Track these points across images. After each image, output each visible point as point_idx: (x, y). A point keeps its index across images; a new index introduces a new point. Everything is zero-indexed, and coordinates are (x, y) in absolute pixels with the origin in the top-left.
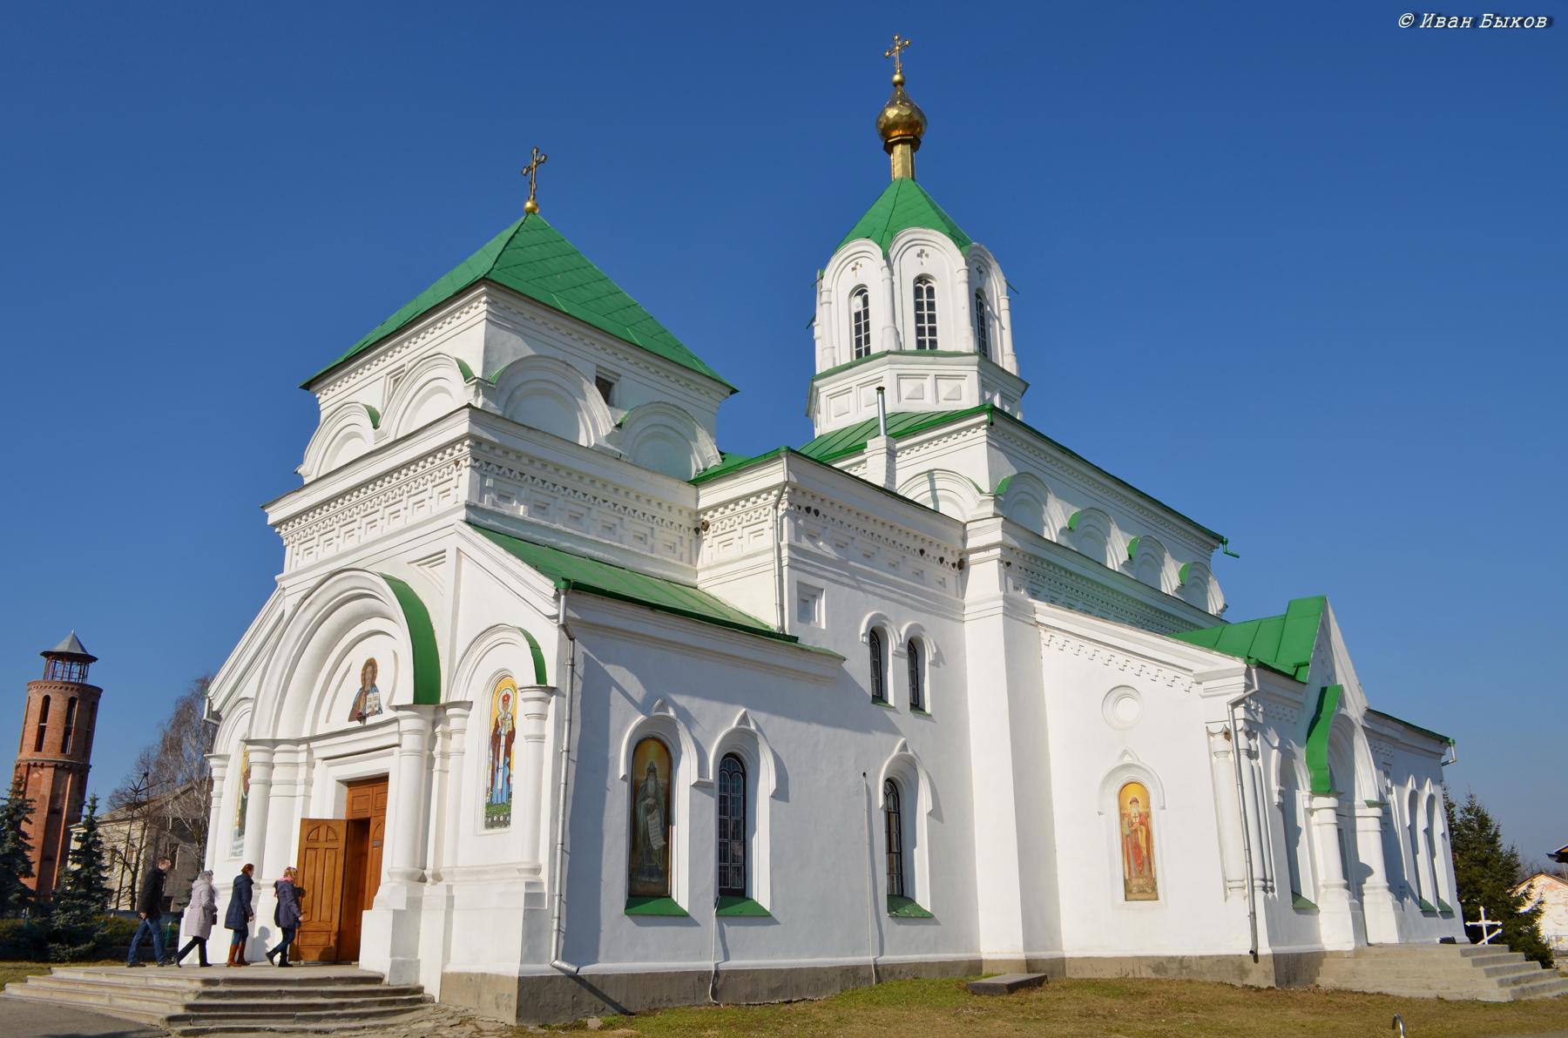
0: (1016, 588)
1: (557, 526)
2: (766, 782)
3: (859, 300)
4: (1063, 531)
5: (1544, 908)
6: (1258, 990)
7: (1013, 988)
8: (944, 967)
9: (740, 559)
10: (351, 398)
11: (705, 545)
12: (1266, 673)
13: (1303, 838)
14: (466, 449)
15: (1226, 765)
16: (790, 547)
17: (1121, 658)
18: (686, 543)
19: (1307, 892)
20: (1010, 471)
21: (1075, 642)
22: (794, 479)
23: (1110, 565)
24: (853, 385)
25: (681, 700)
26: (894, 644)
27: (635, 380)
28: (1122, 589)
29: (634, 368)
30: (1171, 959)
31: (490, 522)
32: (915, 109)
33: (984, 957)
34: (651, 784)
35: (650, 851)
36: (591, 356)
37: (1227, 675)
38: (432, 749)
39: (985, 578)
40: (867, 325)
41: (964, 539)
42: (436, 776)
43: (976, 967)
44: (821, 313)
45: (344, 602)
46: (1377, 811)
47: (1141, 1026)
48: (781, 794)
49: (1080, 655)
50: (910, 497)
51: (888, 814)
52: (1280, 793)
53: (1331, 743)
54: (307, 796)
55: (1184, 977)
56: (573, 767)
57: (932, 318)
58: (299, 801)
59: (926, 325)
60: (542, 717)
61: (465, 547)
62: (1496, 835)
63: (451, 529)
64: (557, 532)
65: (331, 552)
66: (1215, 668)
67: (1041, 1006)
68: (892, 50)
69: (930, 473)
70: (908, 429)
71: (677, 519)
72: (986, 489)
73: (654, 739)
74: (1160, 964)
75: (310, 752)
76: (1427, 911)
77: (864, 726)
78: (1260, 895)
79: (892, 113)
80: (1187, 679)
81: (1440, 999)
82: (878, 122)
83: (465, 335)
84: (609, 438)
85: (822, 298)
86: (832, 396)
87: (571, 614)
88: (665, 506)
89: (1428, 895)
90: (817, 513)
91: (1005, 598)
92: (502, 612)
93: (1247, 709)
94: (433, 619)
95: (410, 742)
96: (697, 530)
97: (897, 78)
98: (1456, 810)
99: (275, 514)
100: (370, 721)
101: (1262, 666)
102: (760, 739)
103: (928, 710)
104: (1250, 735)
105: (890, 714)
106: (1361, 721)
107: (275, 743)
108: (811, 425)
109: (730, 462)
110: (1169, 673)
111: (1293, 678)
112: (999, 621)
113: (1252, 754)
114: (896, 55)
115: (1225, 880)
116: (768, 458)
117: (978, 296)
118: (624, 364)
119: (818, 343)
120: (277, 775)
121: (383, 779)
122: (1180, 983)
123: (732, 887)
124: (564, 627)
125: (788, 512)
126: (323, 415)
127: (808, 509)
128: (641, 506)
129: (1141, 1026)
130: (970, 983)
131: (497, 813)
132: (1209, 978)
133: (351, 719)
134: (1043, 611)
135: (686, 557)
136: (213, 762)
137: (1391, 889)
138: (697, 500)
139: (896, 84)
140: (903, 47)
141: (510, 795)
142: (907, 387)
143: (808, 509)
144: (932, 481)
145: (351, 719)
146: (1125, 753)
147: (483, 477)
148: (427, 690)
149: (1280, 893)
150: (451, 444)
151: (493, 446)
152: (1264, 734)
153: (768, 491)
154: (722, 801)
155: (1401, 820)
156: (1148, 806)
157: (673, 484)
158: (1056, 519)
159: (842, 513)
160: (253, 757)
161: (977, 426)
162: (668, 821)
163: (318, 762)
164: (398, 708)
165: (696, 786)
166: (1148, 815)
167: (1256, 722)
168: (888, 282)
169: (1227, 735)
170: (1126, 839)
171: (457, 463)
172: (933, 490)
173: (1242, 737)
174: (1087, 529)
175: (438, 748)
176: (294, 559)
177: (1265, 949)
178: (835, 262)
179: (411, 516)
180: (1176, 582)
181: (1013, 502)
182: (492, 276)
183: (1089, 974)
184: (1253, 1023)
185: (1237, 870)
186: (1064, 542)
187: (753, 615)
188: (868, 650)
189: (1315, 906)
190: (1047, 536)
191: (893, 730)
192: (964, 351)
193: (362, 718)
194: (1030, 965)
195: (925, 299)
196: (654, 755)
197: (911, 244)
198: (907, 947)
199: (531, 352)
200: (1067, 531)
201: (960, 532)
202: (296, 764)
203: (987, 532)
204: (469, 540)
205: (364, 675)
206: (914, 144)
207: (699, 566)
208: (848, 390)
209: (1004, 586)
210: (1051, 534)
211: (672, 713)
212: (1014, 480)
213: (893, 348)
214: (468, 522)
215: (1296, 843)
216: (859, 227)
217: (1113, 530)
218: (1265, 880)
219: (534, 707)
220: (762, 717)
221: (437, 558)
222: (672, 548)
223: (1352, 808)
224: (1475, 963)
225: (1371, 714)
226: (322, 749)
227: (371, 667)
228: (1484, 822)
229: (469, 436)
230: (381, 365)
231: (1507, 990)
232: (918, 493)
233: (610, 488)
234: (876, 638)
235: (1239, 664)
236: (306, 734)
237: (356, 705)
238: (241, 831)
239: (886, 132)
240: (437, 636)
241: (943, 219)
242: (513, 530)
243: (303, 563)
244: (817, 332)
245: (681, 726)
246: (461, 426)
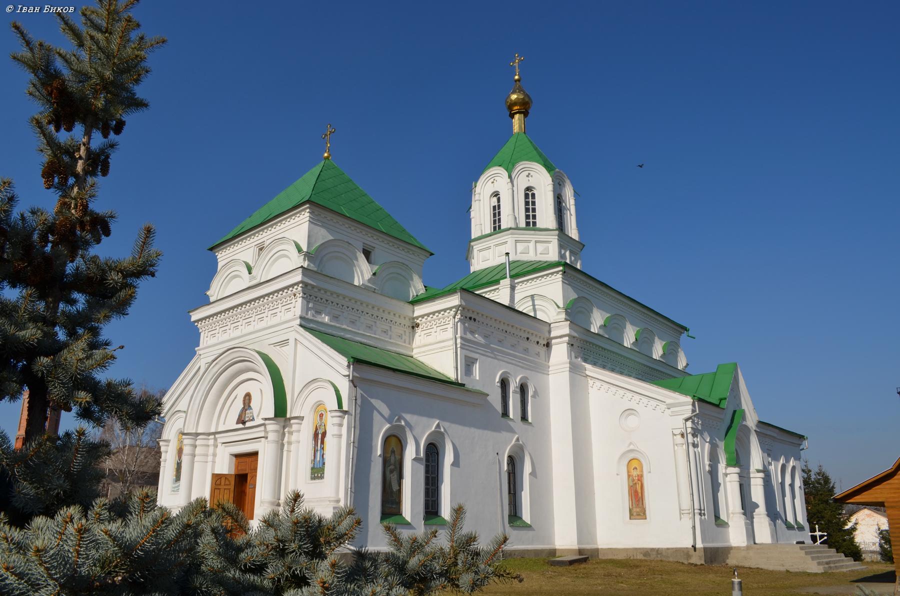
0: (576, 357)
1: (344, 327)
2: (448, 458)
3: (495, 199)
4: (601, 327)
5: (858, 527)
6: (696, 565)
7: (571, 562)
8: (537, 553)
9: (435, 343)
10: (234, 258)
11: (417, 335)
12: (704, 404)
13: (722, 488)
14: (300, 289)
15: (681, 451)
16: (461, 338)
17: (629, 395)
18: (407, 334)
19: (723, 516)
20: (574, 296)
21: (606, 386)
22: (463, 303)
23: (625, 345)
25: (408, 417)
26: (513, 386)
27: (384, 251)
28: (632, 357)
29: (383, 244)
30: (652, 550)
31: (311, 325)
32: (526, 95)
33: (557, 547)
34: (393, 459)
35: (392, 492)
36: (360, 238)
37: (684, 404)
38: (283, 440)
39: (560, 353)
40: (499, 213)
41: (550, 332)
42: (285, 453)
43: (553, 552)
44: (475, 205)
45: (235, 364)
46: (762, 475)
47: (634, 581)
48: (456, 464)
49: (610, 395)
50: (520, 310)
51: (509, 474)
52: (710, 465)
53: (737, 439)
54: (214, 462)
55: (659, 559)
56: (356, 450)
57: (534, 210)
58: (210, 465)
59: (531, 214)
60: (341, 425)
62: (833, 487)
64: (344, 330)
65: (225, 337)
66: (677, 401)
67: (585, 571)
68: (514, 62)
69: (532, 296)
70: (522, 271)
71: (403, 322)
72: (561, 305)
73: (394, 436)
74: (647, 552)
75: (215, 439)
76: (789, 527)
77: (497, 429)
78: (697, 517)
79: (514, 97)
80: (663, 406)
81: (787, 571)
82: (506, 102)
83: (298, 229)
84: (369, 281)
85: (475, 198)
86: (480, 251)
87: (356, 374)
88: (397, 315)
89: (790, 519)
90: (475, 320)
91: (570, 363)
92: (320, 373)
93: (693, 422)
94: (282, 374)
95: (272, 436)
96: (413, 327)
97: (517, 77)
98: (812, 473)
99: (195, 316)
100: (248, 424)
101: (701, 400)
102: (446, 436)
103: (530, 420)
104: (694, 435)
105: (510, 423)
106: (754, 428)
107: (197, 434)
108: (468, 265)
109: (431, 292)
110: (653, 403)
111: (717, 406)
112: (566, 375)
113: (695, 446)
114: (516, 65)
115: (680, 510)
116: (451, 292)
117: (558, 198)
119: (473, 221)
120: (198, 451)
121: (255, 454)
122: (657, 561)
123: (431, 509)
124: (352, 381)
125: (460, 320)
126: (220, 265)
127: (470, 318)
128: (385, 316)
129: (634, 581)
130: (550, 560)
131: (317, 472)
132: (671, 559)
133: (237, 423)
134: (590, 370)
135: (407, 341)
136: (161, 443)
137: (768, 515)
138: (414, 312)
139: (516, 81)
140: (520, 60)
141: (324, 464)
142: (521, 247)
144: (533, 301)
145: (237, 423)
146: (631, 443)
147: (308, 302)
148: (280, 410)
149: (709, 516)
150: (292, 286)
151: (313, 287)
152: (702, 435)
153: (451, 309)
154: (427, 467)
155: (776, 479)
157: (402, 304)
158: (597, 321)
159: (492, 325)
160: (186, 442)
161: (557, 272)
162: (400, 477)
163: (219, 445)
164: (266, 419)
165: (415, 459)
166: (642, 476)
167: (698, 429)
168: (511, 191)
169: (682, 435)
170: (630, 487)
171: (295, 295)
172: (534, 305)
173: (690, 436)
174: (614, 326)
175: (286, 439)
176: (205, 339)
177: (699, 545)
178: (482, 178)
179: (269, 321)
180: (661, 352)
181: (575, 313)
182: (312, 199)
183: (610, 557)
184: (689, 580)
185: (686, 504)
186: (601, 333)
187: (442, 372)
188: (500, 390)
189: (727, 524)
190: (592, 330)
191: (511, 431)
192: (551, 228)
193: (244, 423)
194: (580, 552)
195: (530, 200)
196: (394, 445)
198: (518, 542)
199: (332, 238)
200: (603, 327)
201: (547, 328)
202: (208, 446)
203: (561, 329)
204: (302, 335)
205: (244, 401)
206: (525, 113)
207: (414, 346)
208: (489, 248)
209: (570, 356)
210: (594, 329)
211: (403, 423)
212: (575, 301)
213: (513, 226)
214: (301, 325)
215: (718, 491)
216: (496, 159)
217: (627, 330)
218: (700, 510)
219: (337, 420)
220: (446, 424)
221: (285, 342)
222: (400, 336)
223: (749, 473)
224: (806, 553)
225: (761, 423)
226: (221, 438)
227: (248, 397)
228: (827, 480)
229: (301, 282)
230: (252, 240)
231: (821, 567)
232: (524, 307)
233: (370, 307)
234: (504, 384)
235: (689, 399)
236: (213, 430)
237: (240, 416)
238: (178, 478)
239: (510, 106)
240: (285, 383)
241: (540, 155)
242: (323, 329)
243: (212, 342)
244: (473, 214)
245: (407, 430)
246: (298, 277)
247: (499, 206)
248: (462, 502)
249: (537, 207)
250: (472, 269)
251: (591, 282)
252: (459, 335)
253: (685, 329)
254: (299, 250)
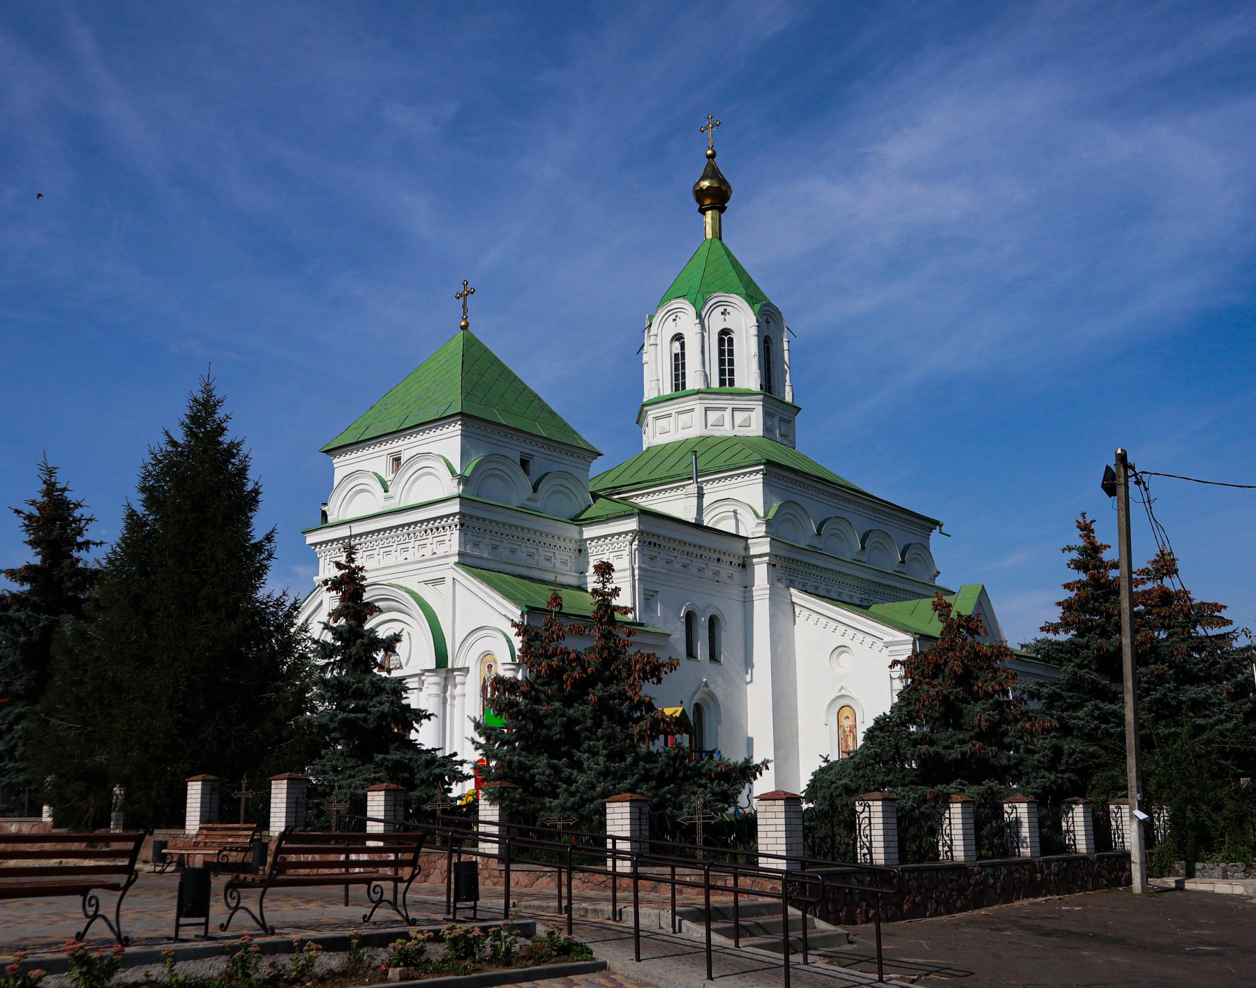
17: (842, 628)
21: (815, 616)
24: (673, 412)
26: (703, 621)
39: (761, 572)
41: (747, 548)
42: (448, 707)
61: (457, 577)
71: (568, 544)
80: (880, 644)
86: (657, 418)
110: (869, 640)
118: (535, 448)
134: (797, 596)
153: (627, 533)
161: (757, 471)
175: (448, 694)
197: (717, 305)
208: (669, 415)
234: (690, 618)
246: (455, 507)
247: (683, 354)
249: (736, 368)
252: (636, 566)
253: (937, 523)
254: (453, 472)
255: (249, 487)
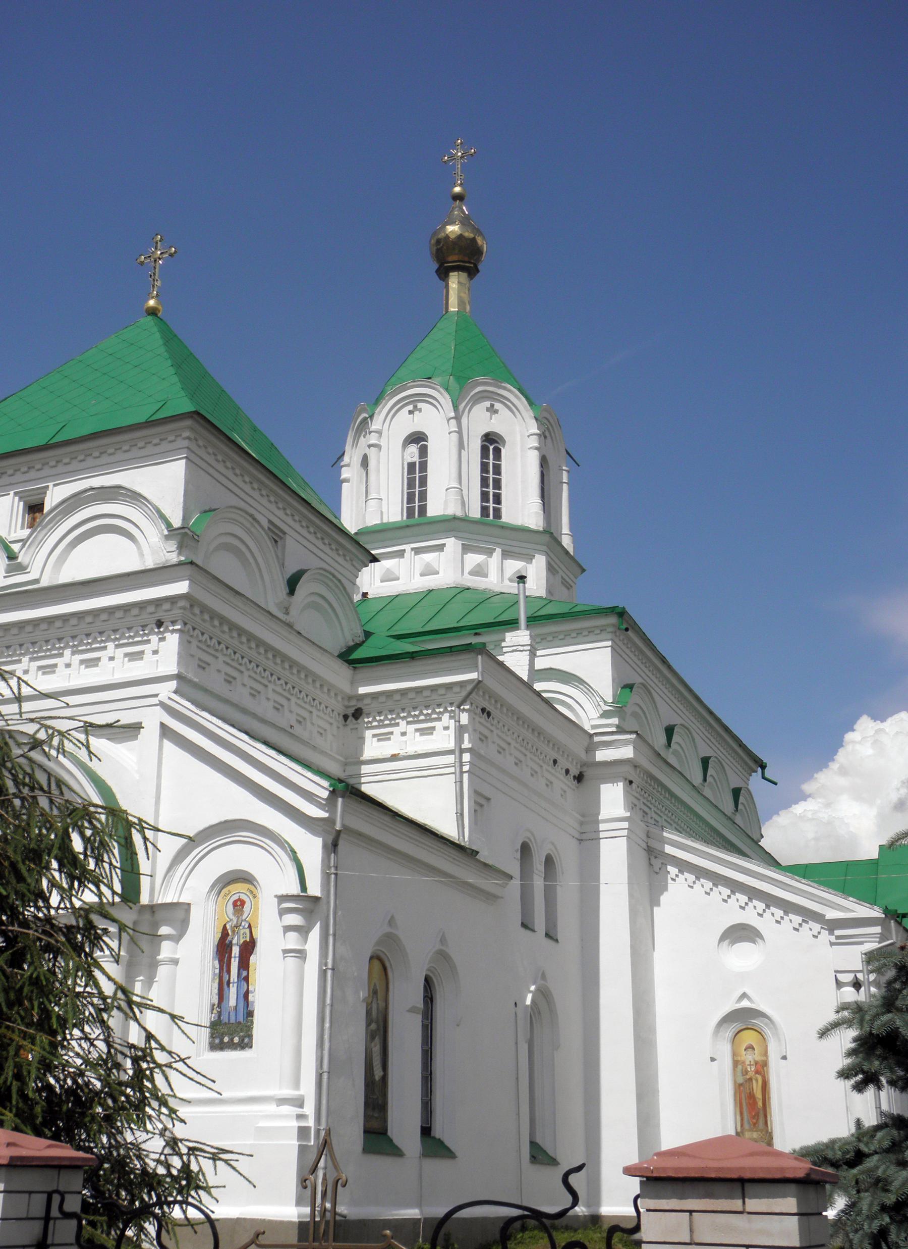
3: (414, 449)
33: (603, 1214)
39: (613, 800)
63: (155, 701)
82: (435, 233)
97: (457, 189)
118: (289, 520)
127: (483, 710)
141: (250, 1014)
143: (483, 710)
146: (744, 996)
156: (766, 1054)
166: (765, 1064)
198: (768, 1149)
208: (401, 554)
247: (424, 466)
248: (834, 1074)
249: (504, 492)
250: (187, 582)
251: (649, 653)
255: (849, 1061)
